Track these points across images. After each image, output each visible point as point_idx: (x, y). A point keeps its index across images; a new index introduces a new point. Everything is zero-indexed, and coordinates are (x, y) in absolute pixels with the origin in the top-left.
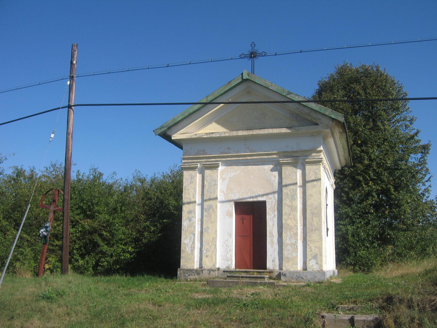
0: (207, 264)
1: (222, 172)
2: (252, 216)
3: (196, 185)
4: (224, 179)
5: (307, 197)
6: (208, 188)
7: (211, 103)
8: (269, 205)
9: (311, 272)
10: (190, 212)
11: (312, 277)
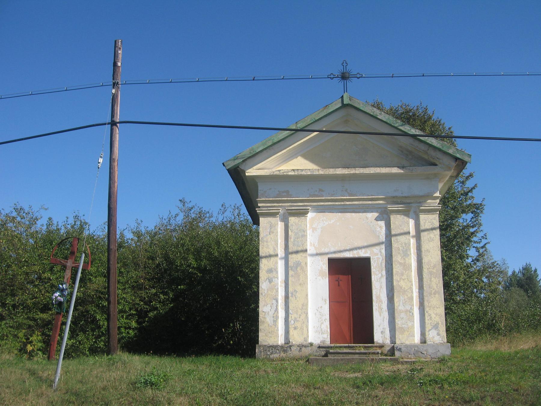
0: (296, 338)
1: (312, 219)
2: (350, 276)
3: (277, 236)
4: (314, 230)
5: (423, 253)
6: (294, 241)
7: (302, 130)
8: (374, 262)
9: (433, 346)
10: (270, 271)
11: (434, 351)
